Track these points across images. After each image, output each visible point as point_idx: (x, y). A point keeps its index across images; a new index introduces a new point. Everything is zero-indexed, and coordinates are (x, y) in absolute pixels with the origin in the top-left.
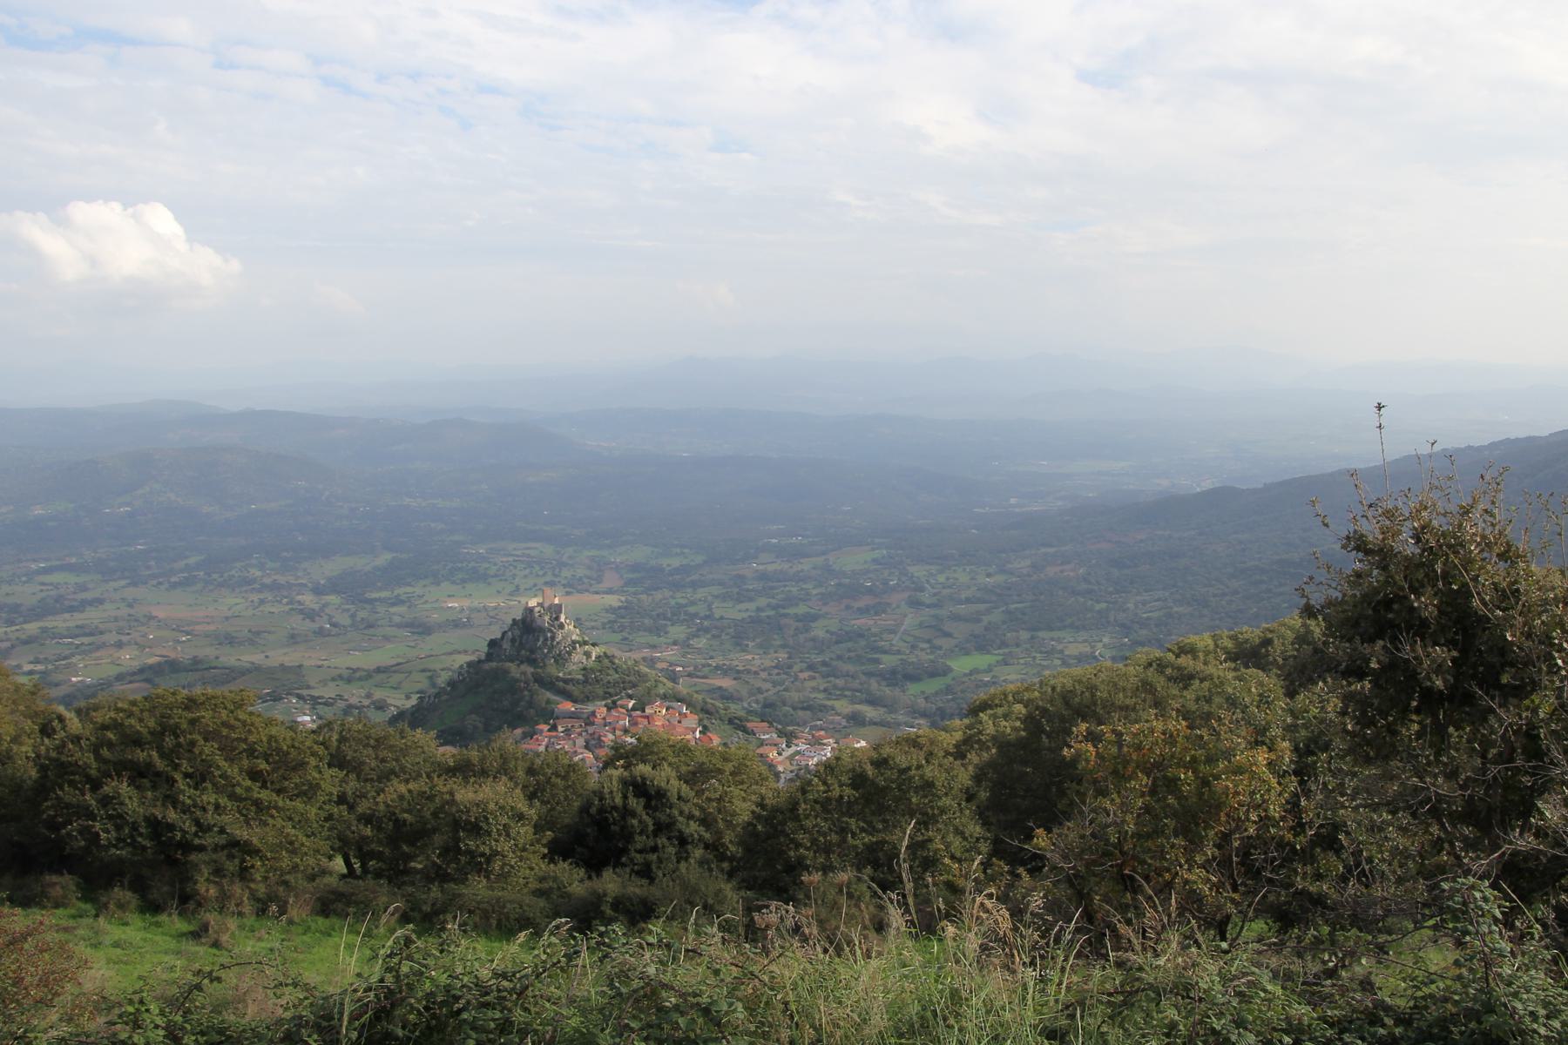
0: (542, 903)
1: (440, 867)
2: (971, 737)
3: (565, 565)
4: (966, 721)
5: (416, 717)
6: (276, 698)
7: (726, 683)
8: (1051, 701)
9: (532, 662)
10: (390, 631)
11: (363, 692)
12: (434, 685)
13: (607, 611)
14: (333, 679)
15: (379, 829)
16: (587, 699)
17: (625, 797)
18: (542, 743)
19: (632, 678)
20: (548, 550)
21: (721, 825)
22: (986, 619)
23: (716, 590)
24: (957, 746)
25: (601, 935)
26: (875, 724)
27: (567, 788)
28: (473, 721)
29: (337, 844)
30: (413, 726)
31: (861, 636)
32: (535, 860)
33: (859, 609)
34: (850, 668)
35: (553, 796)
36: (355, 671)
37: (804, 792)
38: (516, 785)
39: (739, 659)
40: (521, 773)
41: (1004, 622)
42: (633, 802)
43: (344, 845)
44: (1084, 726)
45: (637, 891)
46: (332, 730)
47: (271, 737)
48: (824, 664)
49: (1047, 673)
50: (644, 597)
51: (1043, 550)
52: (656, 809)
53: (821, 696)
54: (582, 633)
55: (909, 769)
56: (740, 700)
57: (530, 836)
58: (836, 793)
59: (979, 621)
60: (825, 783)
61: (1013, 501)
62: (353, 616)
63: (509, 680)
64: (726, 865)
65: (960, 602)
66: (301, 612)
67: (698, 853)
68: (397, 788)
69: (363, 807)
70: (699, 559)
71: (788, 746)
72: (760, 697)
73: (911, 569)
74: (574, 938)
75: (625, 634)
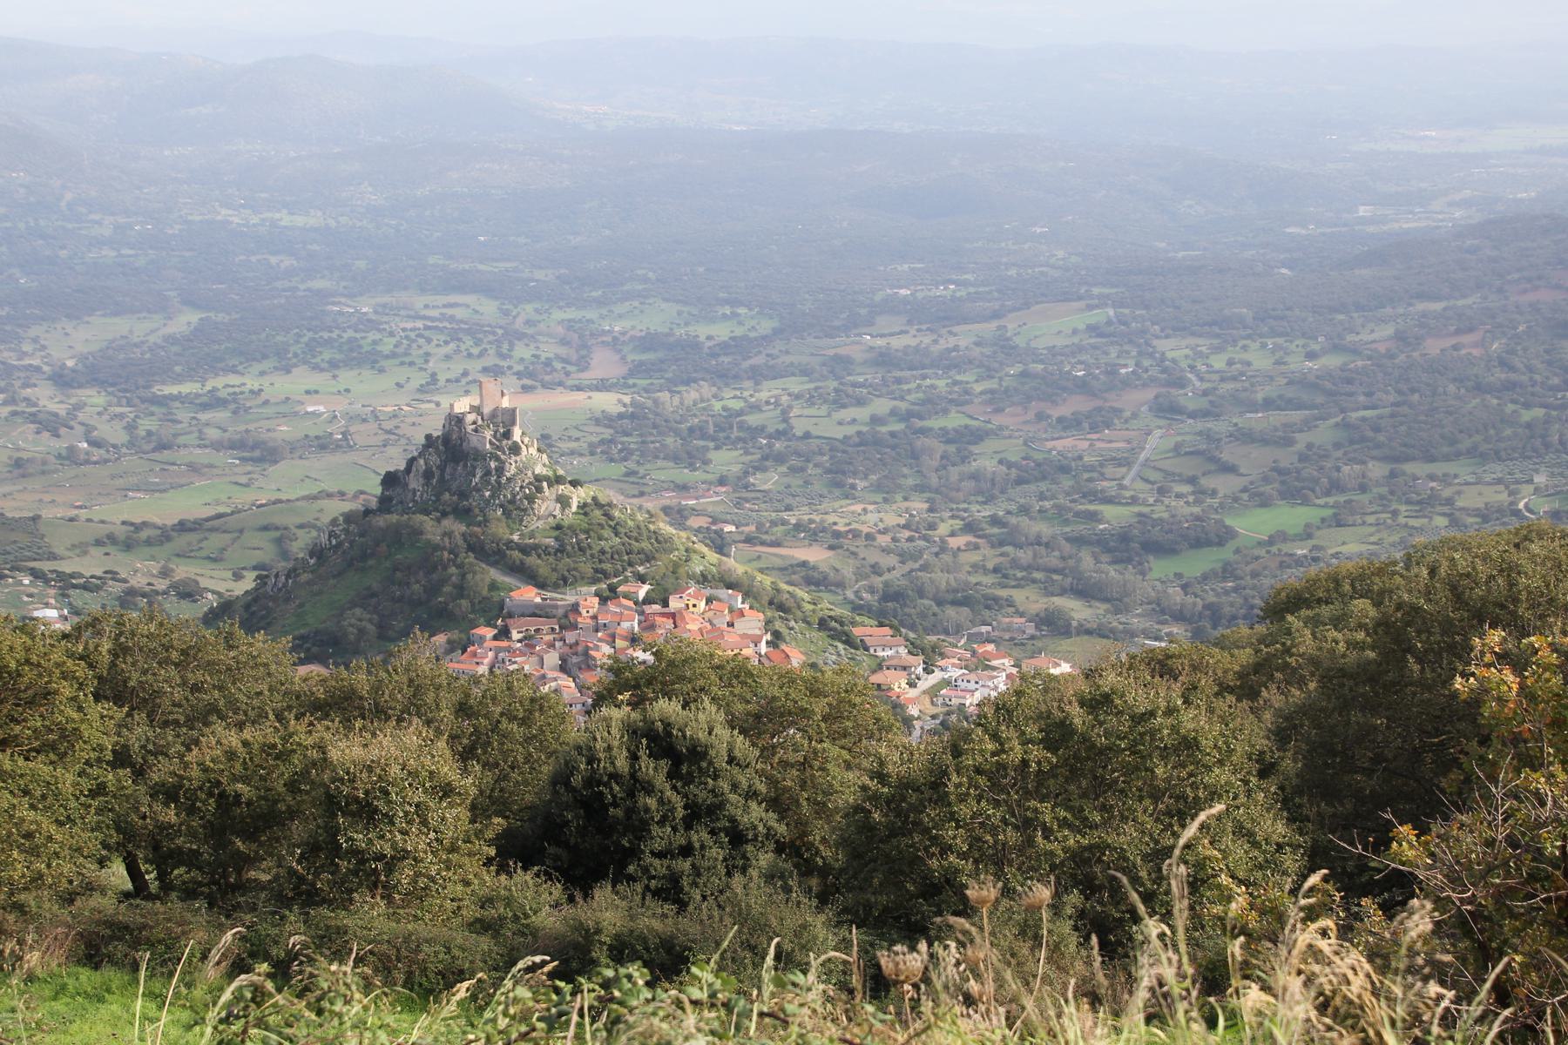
0: (485, 943)
1: (301, 879)
2: (1269, 659)
3: (521, 336)
4: (1261, 629)
5: (254, 612)
7: (815, 555)
8: (1428, 593)
9: (463, 514)
10: (201, 456)
12: (285, 555)
13: (597, 422)
14: (99, 543)
15: (192, 810)
16: (564, 582)
17: (634, 757)
18: (481, 661)
19: (645, 545)
21: (805, 808)
22: (1302, 439)
23: (796, 385)
24: (1241, 675)
25: (607, 985)
26: (1089, 632)
27: (528, 740)
28: (357, 620)
29: (115, 838)
30: (250, 627)
31: (1065, 469)
32: (472, 867)
33: (1060, 420)
34: (1043, 528)
37: (957, 752)
38: (439, 732)
39: (841, 514)
40: (446, 713)
41: (1337, 446)
42: (647, 766)
43: (127, 841)
44: (1495, 637)
45: (657, 924)
46: (99, 633)
48: (995, 521)
49: (1419, 540)
50: (664, 396)
51: (1421, 306)
52: (689, 779)
53: (988, 580)
55: (1152, 714)
57: (464, 825)
58: (1016, 753)
59: (1289, 442)
60: (995, 737)
61: (1363, 211)
62: (131, 428)
63: (421, 546)
64: (814, 882)
65: (1253, 407)
66: (33, 418)
67: (765, 859)
68: (222, 738)
69: (161, 772)
70: (766, 326)
71: (928, 671)
72: (878, 581)
73: (1163, 345)
74: (557, 991)
75: (631, 465)
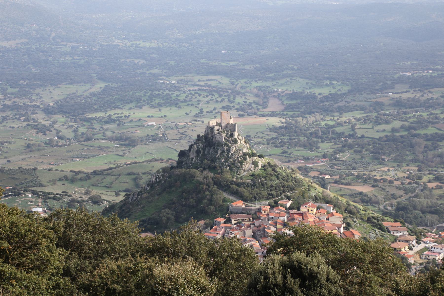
3: (238, 93)
5: (123, 210)
6: (16, 193)
7: (366, 189)
9: (212, 169)
10: (104, 143)
11: (83, 190)
12: (137, 185)
13: (271, 130)
14: (60, 180)
16: (255, 199)
17: (285, 277)
19: (290, 183)
20: (225, 81)
23: (358, 114)
27: (239, 268)
30: (122, 217)
35: (229, 274)
36: (77, 173)
37: (433, 281)
38: (200, 264)
40: (204, 255)
46: (59, 218)
47: (12, 224)
50: (300, 119)
54: (251, 148)
56: (377, 203)
62: (75, 131)
63: (198, 180)
66: (35, 127)
68: (110, 264)
69: (83, 279)
70: (345, 89)
71: (418, 243)
72: (395, 202)
75: (285, 149)
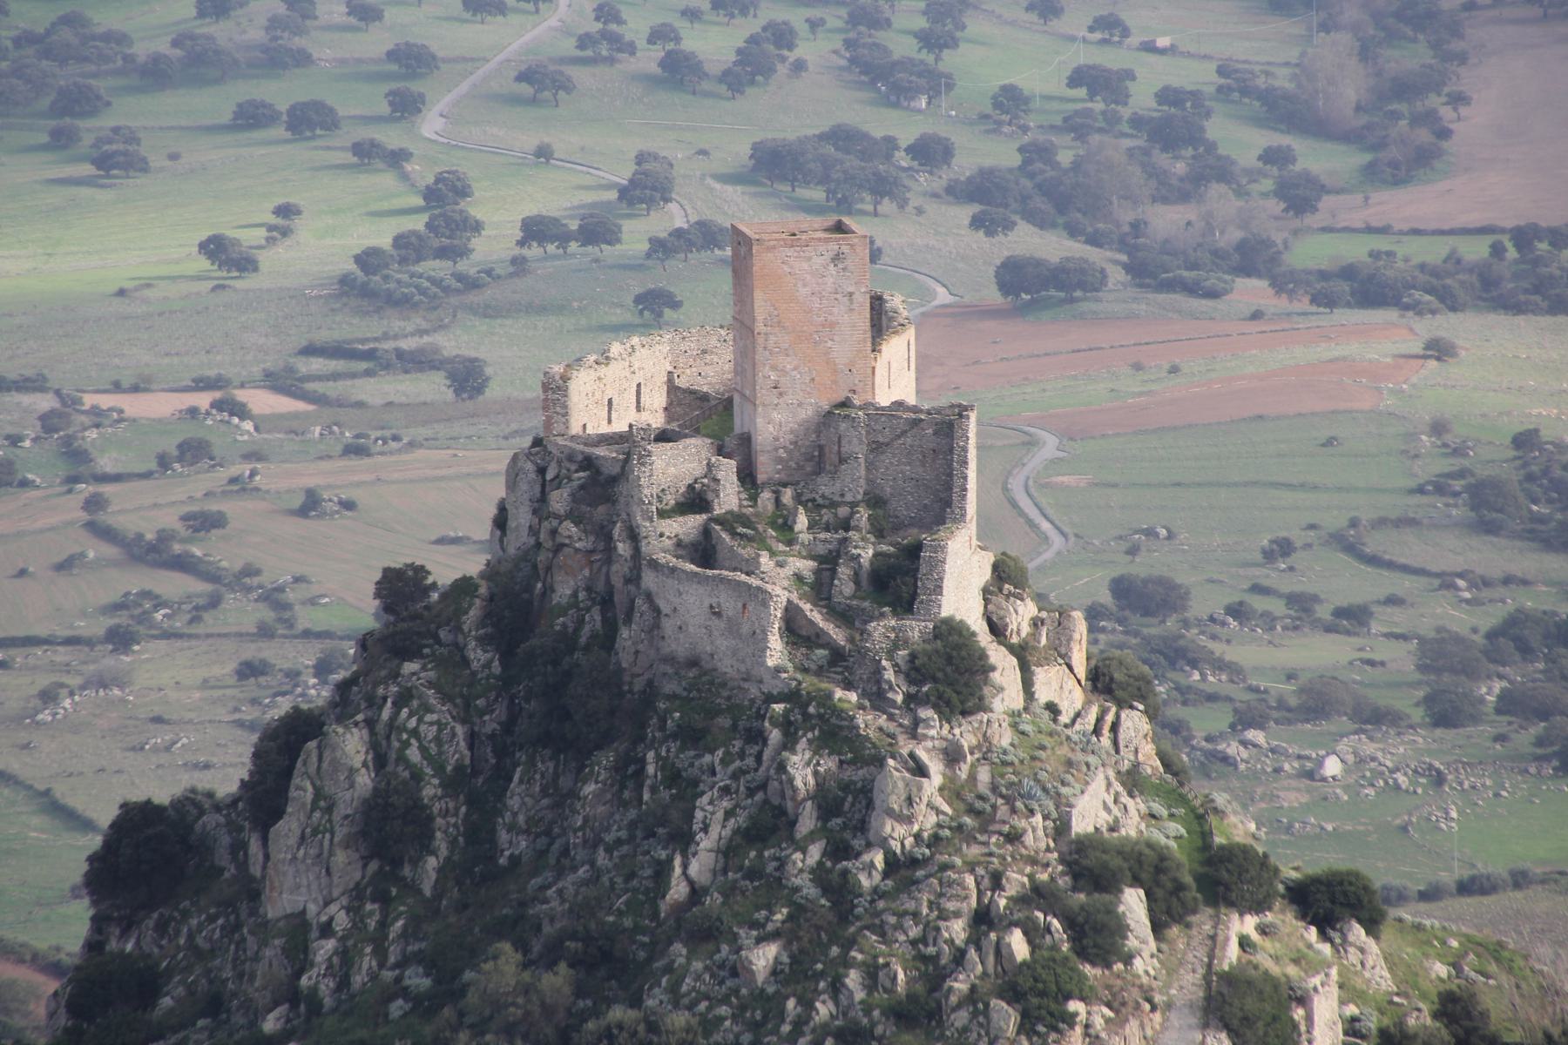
54: (1172, 783)
